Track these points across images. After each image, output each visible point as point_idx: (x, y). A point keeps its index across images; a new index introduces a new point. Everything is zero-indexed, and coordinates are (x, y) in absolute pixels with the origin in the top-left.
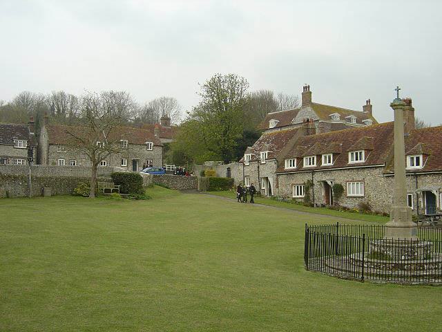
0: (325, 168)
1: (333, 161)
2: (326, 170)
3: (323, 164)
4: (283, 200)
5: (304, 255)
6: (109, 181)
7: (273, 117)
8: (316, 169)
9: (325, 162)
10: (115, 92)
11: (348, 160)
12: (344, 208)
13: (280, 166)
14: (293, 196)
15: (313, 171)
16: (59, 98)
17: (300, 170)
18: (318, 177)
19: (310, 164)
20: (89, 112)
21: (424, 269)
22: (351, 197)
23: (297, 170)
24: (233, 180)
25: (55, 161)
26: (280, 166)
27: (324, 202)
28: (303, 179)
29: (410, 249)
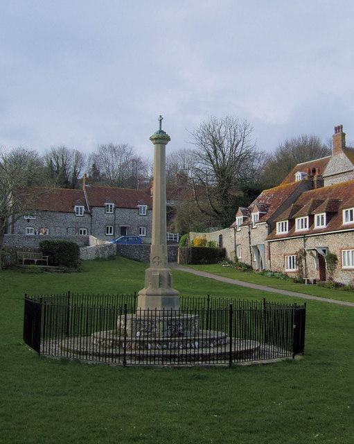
0: (319, 231)
1: (327, 222)
2: (318, 234)
3: (316, 227)
4: (273, 276)
5: (22, 330)
6: (35, 251)
7: (301, 169)
8: (308, 233)
9: (318, 225)
10: (115, 144)
11: (342, 221)
12: (338, 285)
13: (272, 228)
14: (287, 270)
15: (304, 236)
16: (62, 154)
17: (292, 235)
18: (312, 243)
19: (302, 228)
20: (221, 172)
21: (147, 349)
22: (345, 270)
23: (288, 236)
24: (224, 250)
25: (22, 230)
26: (272, 228)
27: (318, 277)
28: (294, 246)
29: (146, 323)
